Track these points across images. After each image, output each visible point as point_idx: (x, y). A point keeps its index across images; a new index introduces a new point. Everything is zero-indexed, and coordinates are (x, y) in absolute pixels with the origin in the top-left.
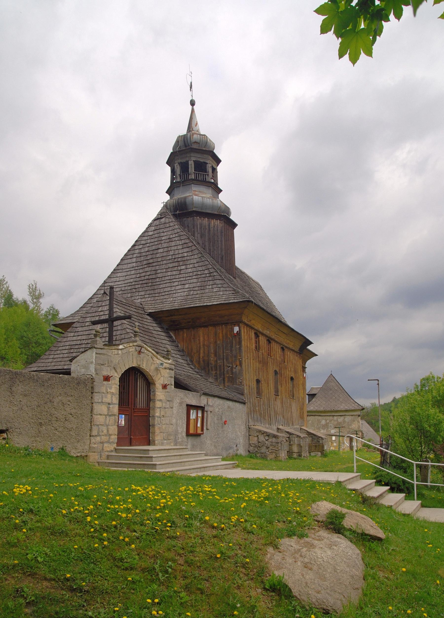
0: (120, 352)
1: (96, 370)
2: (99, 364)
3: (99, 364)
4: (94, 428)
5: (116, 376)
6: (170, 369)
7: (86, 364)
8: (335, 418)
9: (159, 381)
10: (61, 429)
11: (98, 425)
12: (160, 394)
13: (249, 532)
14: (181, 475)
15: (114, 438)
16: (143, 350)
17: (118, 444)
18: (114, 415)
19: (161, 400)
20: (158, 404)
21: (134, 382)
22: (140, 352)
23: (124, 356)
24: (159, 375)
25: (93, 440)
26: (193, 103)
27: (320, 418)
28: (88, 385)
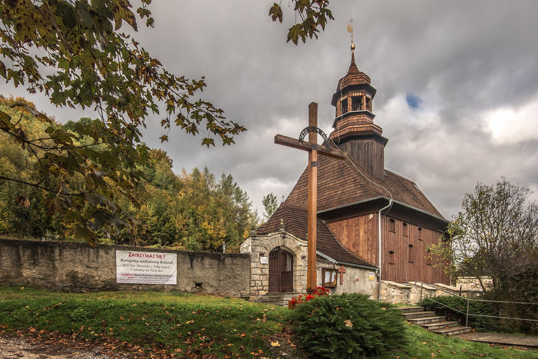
0: (269, 238)
1: (252, 249)
2: (254, 246)
3: (254, 246)
5: (267, 253)
13: (381, 319)
14: (139, 305)
15: (266, 288)
16: (286, 236)
18: (266, 275)
22: (284, 238)
23: (273, 240)
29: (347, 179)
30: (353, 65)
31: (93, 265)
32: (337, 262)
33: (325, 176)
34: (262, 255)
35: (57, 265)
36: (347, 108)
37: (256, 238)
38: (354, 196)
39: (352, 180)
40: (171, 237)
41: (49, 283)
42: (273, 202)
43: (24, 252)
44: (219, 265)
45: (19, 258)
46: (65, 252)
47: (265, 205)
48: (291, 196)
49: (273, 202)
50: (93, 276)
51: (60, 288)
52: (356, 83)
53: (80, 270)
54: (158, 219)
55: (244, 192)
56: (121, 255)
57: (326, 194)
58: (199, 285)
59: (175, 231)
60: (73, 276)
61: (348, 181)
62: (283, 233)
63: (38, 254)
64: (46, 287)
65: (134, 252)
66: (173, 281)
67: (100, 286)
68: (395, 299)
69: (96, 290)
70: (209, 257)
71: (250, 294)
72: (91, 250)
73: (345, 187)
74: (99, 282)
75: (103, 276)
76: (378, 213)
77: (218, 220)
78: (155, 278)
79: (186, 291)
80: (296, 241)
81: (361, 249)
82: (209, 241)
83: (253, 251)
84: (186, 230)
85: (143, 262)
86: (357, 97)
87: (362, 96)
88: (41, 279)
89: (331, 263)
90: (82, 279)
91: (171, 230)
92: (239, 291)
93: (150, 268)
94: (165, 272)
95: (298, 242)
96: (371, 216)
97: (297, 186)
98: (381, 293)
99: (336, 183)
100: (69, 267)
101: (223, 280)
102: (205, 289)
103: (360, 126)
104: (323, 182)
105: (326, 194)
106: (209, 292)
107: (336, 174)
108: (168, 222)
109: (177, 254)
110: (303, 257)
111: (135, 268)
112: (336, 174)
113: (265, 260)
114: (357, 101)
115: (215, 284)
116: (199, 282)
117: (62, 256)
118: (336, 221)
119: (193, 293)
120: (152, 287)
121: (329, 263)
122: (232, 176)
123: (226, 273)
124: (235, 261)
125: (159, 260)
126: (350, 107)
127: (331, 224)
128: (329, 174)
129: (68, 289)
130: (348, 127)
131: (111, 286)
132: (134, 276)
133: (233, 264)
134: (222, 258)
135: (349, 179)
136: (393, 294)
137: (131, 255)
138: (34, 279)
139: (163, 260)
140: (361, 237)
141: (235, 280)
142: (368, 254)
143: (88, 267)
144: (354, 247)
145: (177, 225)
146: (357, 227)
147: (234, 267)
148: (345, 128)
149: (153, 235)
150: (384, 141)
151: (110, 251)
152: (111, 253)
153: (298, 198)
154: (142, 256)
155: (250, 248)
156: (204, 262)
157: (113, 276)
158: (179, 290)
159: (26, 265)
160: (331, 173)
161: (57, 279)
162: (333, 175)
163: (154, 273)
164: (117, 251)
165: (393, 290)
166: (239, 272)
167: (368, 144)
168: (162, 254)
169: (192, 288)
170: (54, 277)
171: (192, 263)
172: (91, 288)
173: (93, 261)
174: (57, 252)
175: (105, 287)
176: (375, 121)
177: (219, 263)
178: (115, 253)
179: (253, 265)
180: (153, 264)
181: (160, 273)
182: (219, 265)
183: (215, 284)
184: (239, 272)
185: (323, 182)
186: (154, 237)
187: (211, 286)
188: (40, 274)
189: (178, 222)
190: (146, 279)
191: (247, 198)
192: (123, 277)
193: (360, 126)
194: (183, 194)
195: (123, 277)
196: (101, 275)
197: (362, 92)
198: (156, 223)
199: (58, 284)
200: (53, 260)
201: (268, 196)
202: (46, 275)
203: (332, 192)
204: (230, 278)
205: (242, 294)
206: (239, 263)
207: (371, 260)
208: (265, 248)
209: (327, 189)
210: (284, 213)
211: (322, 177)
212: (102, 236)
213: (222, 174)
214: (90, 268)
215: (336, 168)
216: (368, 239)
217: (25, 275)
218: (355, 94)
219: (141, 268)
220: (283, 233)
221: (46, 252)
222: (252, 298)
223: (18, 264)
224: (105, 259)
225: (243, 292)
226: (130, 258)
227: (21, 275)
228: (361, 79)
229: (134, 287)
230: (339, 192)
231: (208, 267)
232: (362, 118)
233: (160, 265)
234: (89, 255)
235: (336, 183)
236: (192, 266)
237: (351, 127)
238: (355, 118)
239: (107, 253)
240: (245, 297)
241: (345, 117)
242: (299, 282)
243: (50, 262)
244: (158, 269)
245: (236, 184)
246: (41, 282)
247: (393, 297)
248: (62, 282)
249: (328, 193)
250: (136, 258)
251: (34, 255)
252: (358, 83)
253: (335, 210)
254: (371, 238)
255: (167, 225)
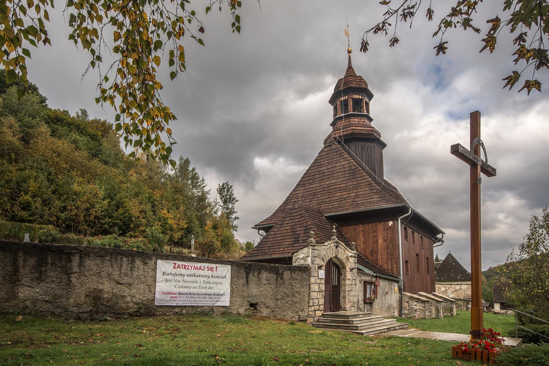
1: (312, 261)
4: (311, 301)
6: (355, 257)
7: (303, 257)
8: (453, 286)
9: (348, 266)
10: (290, 303)
11: (313, 299)
12: (349, 275)
15: (322, 307)
17: (324, 311)
18: (322, 291)
19: (349, 279)
20: (348, 282)
21: (334, 267)
22: (337, 247)
24: (348, 262)
25: (310, 309)
26: (349, 52)
27: (440, 286)
28: (305, 270)
29: (360, 182)
30: (350, 68)
31: (126, 280)
32: (375, 274)
33: (334, 175)
34: (320, 267)
35: (74, 280)
36: (347, 109)
37: (316, 248)
38: (371, 200)
39: (367, 183)
40: (124, 225)
41: (59, 307)
42: (228, 190)
43: (25, 261)
44: (277, 280)
45: (16, 270)
46: (88, 262)
47: (220, 194)
48: (294, 193)
49: (228, 190)
50: (124, 297)
51: (74, 315)
52: (355, 86)
53: (107, 287)
54: (109, 203)
55: (201, 179)
56: (164, 266)
57: (337, 195)
58: (253, 305)
59: (130, 218)
60: (96, 297)
61: (362, 184)
62: (336, 242)
63: (47, 263)
64: (53, 314)
65: (180, 263)
66: (225, 301)
67: (131, 311)
68: (418, 313)
69: (126, 316)
70: (267, 271)
71: (308, 316)
72: (125, 259)
73: (359, 190)
74: (131, 305)
75: (138, 296)
76: (398, 220)
77: (177, 208)
78: (204, 298)
79: (239, 314)
80: (346, 251)
81: (380, 257)
82: (168, 232)
83: (312, 264)
84: (143, 218)
85: (191, 275)
86: (357, 99)
87: (361, 100)
88: (46, 302)
89: (368, 275)
90: (108, 301)
91: (125, 217)
92: (297, 312)
93: (199, 284)
94: (217, 289)
95: (348, 252)
96: (391, 223)
97: (301, 183)
98: (312, 289)
99: (348, 184)
100: (92, 284)
101: (281, 299)
102: (260, 311)
103: (363, 128)
104: (333, 181)
105: (337, 195)
106: (264, 314)
107: (348, 175)
108: (122, 207)
109: (232, 266)
110: (351, 270)
111: (180, 284)
112: (348, 175)
113: (322, 273)
114: (358, 104)
115: (272, 304)
116: (254, 301)
117: (82, 268)
118: (350, 225)
119: (248, 316)
120: (199, 310)
121: (368, 275)
122: (190, 159)
123: (285, 290)
124: (294, 275)
125: (210, 273)
126: (350, 107)
127: (344, 228)
128: (339, 174)
129: (85, 315)
130: (351, 128)
131: (147, 311)
132: (178, 295)
133: (292, 278)
134: (280, 272)
135: (362, 181)
136: (416, 307)
137: (176, 266)
138: (35, 301)
139: (215, 273)
140: (380, 244)
141: (294, 299)
142: (388, 263)
143: (118, 283)
144: (372, 255)
145: (133, 212)
146: (375, 234)
147: (293, 283)
148: (348, 129)
149: (103, 222)
150: (384, 145)
151: (150, 261)
152: (151, 263)
153: (302, 197)
154: (190, 268)
155: (309, 260)
156: (260, 276)
157: (150, 296)
158: (231, 313)
159: (25, 281)
160: (341, 174)
161: (71, 301)
162: (344, 176)
163: (203, 291)
164: (159, 261)
165: (415, 303)
166: (298, 289)
167: (371, 147)
168: (214, 266)
169: (246, 310)
170: (67, 299)
171: (247, 277)
172: (119, 314)
173: (126, 275)
174: (76, 260)
175: (138, 311)
176: (372, 124)
177: (277, 277)
178: (156, 263)
179: (313, 280)
180: (202, 279)
181: (209, 291)
182: (277, 280)
183: (272, 304)
184: (298, 289)
185: (333, 181)
186: (104, 224)
187: (267, 307)
188: (46, 293)
189: (134, 207)
190: (192, 299)
191: (204, 185)
192: (163, 297)
193: (363, 128)
194: (135, 175)
195: (163, 297)
196: (134, 295)
197: (362, 96)
198: (106, 207)
199: (71, 309)
200: (68, 273)
201: (224, 184)
202: (54, 296)
203: (344, 193)
204: (288, 296)
205: (299, 316)
206: (298, 277)
207: (392, 270)
208: (323, 259)
209: (338, 189)
210: (300, 213)
211: (330, 176)
212: (35, 220)
213: (179, 157)
214: (120, 284)
215: (346, 169)
216: (388, 248)
217: (21, 295)
218: (355, 96)
219: (188, 285)
220: (336, 242)
221: (59, 261)
222: (310, 320)
223: (14, 279)
224: (141, 272)
225: (301, 313)
226: (178, 271)
227: (15, 296)
228: (360, 83)
229: (177, 310)
230: (352, 195)
231: (266, 282)
232: (362, 120)
233: (211, 280)
234: (121, 266)
235: (348, 184)
236: (247, 282)
237: (354, 128)
238: (356, 120)
239: (146, 264)
240: (303, 320)
241: (346, 117)
242: (348, 299)
243: (65, 276)
244: (208, 285)
245: (194, 169)
246: (46, 307)
247: (416, 311)
248: (78, 305)
249: (339, 194)
250: (183, 271)
251: (41, 265)
252: (358, 86)
253: (352, 213)
254: (390, 246)
255: (121, 211)
